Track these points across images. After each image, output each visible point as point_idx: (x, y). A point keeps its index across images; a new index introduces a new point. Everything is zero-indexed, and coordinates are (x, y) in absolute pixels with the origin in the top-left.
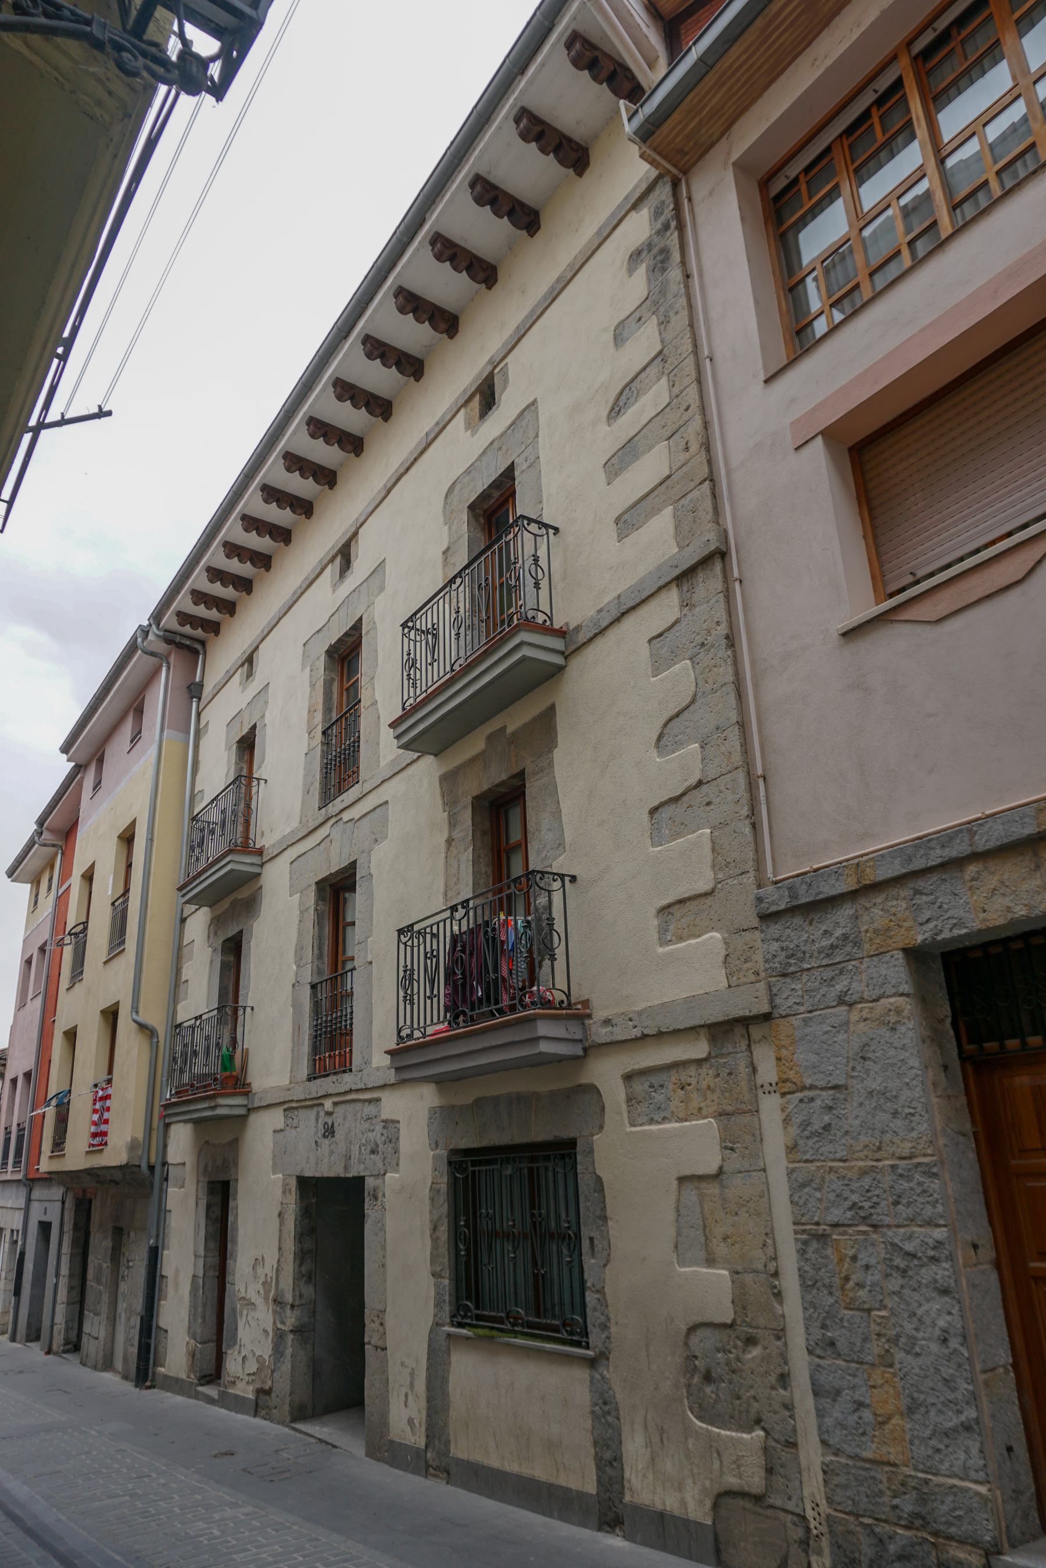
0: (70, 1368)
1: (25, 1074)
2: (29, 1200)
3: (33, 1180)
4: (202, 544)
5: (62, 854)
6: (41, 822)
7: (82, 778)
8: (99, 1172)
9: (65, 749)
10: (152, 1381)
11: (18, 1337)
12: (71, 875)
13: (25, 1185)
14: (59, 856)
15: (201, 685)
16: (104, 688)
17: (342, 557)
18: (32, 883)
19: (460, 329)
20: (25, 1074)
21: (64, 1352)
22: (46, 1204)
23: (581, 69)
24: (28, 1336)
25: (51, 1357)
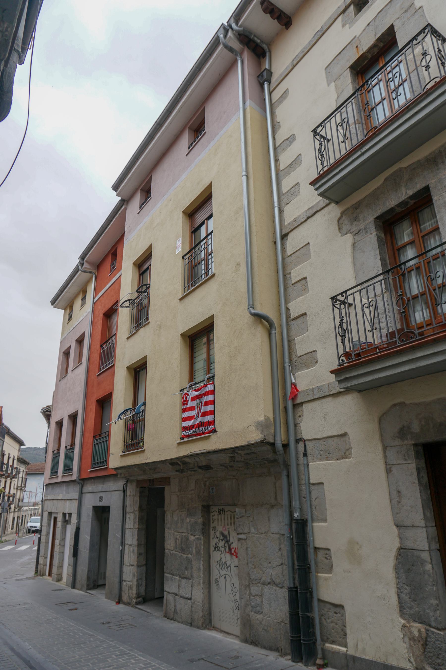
0: (152, 617)
1: (70, 416)
2: (81, 493)
3: (83, 480)
4: (197, 67)
5: (96, 278)
6: (83, 257)
7: (126, 209)
8: (187, 460)
9: (115, 188)
10: (323, 658)
11: (78, 585)
12: (121, 268)
13: (79, 483)
14: (94, 278)
15: (270, 73)
16: (150, 136)
17: (354, 5)
18: (65, 309)
19: (293, 23)
20: (70, 416)
21: (137, 603)
22: (101, 494)
23: (266, 13)
24: (88, 585)
25: (121, 606)
